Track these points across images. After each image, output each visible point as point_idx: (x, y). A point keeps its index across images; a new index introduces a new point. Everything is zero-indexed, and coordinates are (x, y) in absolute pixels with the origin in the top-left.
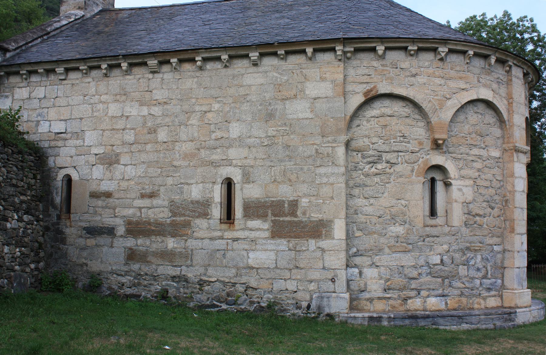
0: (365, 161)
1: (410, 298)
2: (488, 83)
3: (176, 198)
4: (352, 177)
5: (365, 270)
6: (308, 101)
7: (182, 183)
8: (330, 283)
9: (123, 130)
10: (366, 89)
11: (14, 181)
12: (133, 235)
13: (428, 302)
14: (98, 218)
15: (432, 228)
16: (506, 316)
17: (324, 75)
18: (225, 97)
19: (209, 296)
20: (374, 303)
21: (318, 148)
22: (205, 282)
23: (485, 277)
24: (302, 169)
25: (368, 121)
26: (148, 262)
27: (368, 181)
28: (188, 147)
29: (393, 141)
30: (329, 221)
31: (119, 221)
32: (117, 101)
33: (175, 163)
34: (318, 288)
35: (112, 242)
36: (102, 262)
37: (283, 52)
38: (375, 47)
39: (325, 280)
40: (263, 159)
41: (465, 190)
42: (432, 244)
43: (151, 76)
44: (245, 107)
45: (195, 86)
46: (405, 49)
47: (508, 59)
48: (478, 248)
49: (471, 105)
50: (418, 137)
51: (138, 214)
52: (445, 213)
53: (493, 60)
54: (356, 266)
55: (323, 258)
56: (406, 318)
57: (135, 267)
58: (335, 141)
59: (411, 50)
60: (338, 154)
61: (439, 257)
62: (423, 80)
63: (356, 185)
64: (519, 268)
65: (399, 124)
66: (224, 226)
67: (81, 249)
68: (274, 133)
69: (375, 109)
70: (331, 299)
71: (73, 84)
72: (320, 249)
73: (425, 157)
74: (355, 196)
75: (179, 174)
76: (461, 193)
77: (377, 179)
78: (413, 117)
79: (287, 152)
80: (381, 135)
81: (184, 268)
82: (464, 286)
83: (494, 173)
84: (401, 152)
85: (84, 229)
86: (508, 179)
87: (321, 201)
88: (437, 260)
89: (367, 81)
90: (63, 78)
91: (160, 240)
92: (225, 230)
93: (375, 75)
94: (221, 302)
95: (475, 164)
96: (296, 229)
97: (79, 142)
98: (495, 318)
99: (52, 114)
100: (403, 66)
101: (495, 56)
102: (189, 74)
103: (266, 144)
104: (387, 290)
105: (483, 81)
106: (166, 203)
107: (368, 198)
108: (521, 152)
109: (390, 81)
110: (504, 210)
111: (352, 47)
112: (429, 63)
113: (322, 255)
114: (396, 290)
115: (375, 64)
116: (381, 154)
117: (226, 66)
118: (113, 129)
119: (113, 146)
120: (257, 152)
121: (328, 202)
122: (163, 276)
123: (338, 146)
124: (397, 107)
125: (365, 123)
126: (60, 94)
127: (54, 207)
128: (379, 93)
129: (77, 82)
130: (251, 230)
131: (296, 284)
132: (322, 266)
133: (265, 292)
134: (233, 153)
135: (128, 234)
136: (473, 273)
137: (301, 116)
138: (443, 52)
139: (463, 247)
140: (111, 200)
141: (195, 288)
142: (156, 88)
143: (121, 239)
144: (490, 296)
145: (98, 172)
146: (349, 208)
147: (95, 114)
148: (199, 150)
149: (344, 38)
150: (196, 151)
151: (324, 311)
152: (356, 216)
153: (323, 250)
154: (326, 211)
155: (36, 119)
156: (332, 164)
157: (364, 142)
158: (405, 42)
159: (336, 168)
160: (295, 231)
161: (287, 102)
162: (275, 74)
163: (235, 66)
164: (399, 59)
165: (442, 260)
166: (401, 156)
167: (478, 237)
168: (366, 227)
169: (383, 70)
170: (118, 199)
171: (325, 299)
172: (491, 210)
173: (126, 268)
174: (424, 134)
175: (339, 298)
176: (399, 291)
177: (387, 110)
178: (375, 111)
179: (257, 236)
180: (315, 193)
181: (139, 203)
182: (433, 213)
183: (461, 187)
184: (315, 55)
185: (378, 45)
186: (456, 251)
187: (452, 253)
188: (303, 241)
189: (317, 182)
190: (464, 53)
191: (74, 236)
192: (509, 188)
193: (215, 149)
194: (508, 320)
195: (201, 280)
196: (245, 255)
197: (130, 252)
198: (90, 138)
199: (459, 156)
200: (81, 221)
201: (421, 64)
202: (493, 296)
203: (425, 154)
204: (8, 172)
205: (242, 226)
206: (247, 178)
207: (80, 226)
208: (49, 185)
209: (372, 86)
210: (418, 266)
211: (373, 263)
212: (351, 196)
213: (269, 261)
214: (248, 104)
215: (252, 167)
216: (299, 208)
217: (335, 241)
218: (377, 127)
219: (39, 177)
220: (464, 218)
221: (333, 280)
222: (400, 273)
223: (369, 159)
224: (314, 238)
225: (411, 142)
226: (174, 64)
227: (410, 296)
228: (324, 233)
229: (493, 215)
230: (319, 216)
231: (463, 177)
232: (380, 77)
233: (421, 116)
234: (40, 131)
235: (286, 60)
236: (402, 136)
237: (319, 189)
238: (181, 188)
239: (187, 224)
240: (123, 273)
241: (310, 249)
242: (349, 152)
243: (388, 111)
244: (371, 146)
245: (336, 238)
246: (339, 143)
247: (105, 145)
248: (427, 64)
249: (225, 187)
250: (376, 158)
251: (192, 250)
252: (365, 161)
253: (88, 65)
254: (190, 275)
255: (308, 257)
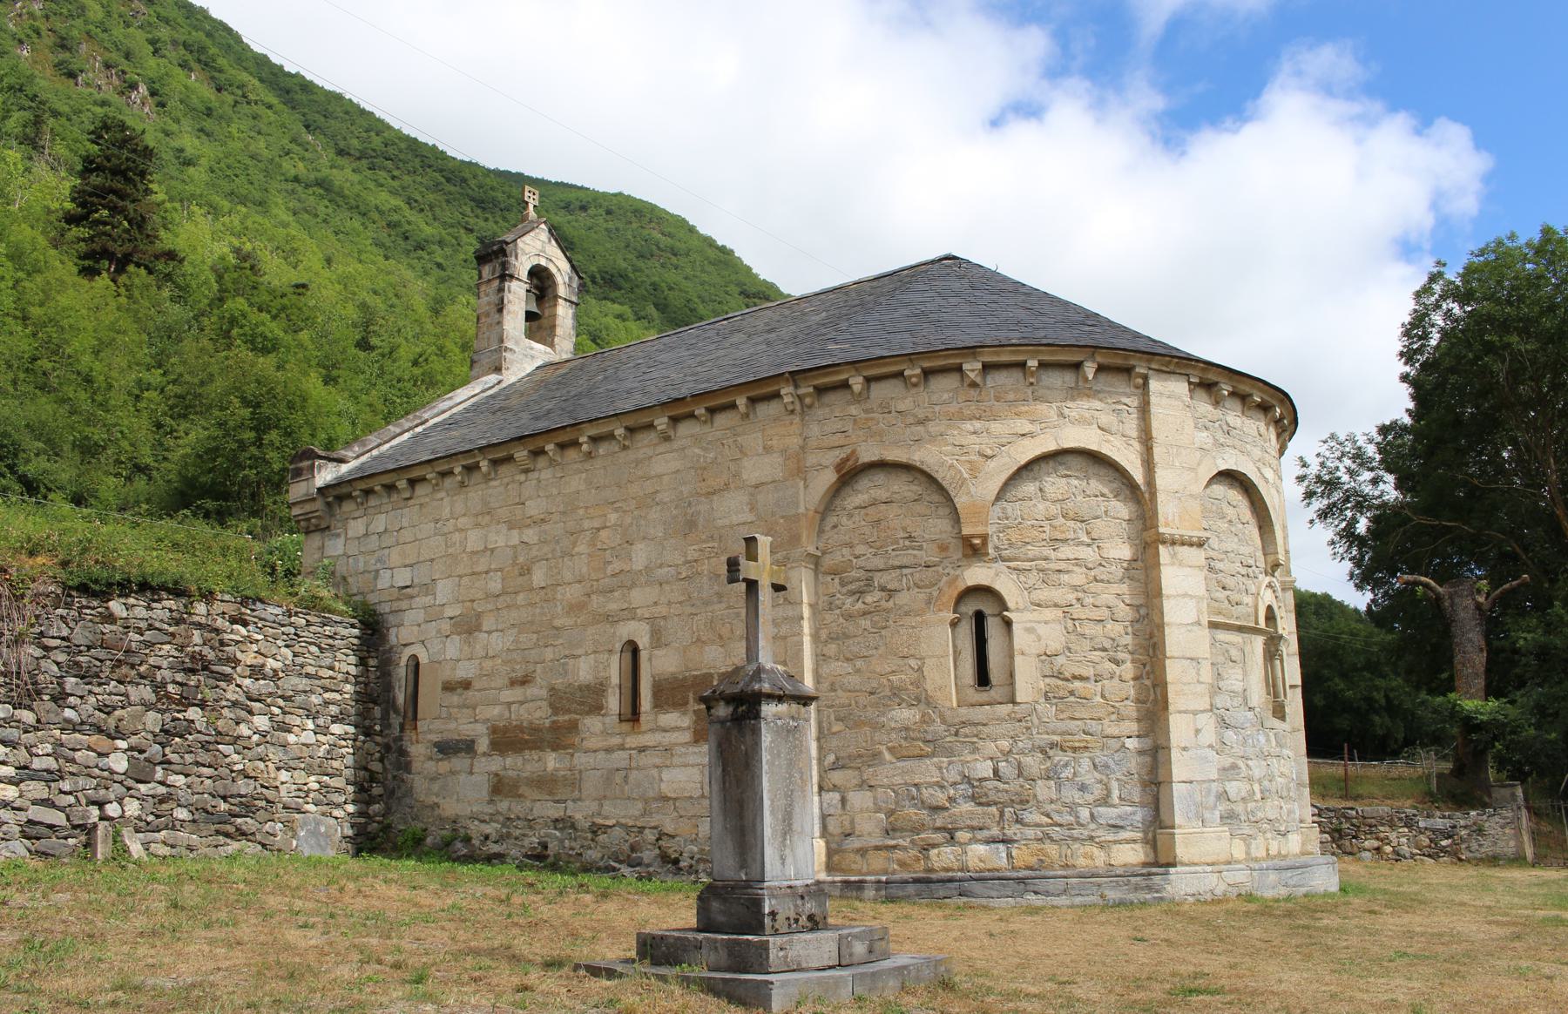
0: (844, 590)
1: (934, 846)
2: (1087, 415)
3: (559, 682)
5: (851, 796)
7: (566, 656)
9: (487, 573)
11: (310, 670)
12: (500, 751)
13: (970, 853)
14: (453, 725)
15: (971, 709)
18: (625, 500)
19: (605, 851)
22: (601, 827)
23: (1105, 801)
25: (850, 516)
26: (520, 796)
28: (572, 593)
31: (481, 729)
32: (477, 525)
33: (558, 623)
35: (472, 765)
36: (458, 800)
37: (1036, 364)
38: (847, 380)
40: (680, 603)
41: (1042, 630)
43: (522, 477)
44: (654, 514)
45: (582, 487)
46: (899, 375)
47: (1132, 362)
48: (1082, 745)
49: (1051, 463)
51: (507, 714)
53: (1090, 369)
54: (835, 788)
57: (503, 805)
59: (911, 376)
61: (989, 763)
64: (1191, 782)
66: (626, 727)
67: (432, 779)
68: (696, 555)
69: (860, 492)
71: (421, 505)
73: (952, 572)
75: (561, 641)
77: (865, 623)
79: (716, 587)
81: (570, 803)
82: (1050, 821)
84: (906, 567)
85: (436, 745)
88: (984, 769)
89: (841, 443)
90: (408, 496)
91: (536, 758)
92: (627, 734)
94: (621, 862)
95: (1065, 578)
97: (428, 600)
99: (395, 557)
100: (901, 407)
101: (1094, 361)
102: (576, 466)
103: (684, 575)
106: (544, 693)
108: (1183, 544)
114: (906, 830)
117: (625, 448)
118: (473, 574)
119: (473, 601)
120: (672, 591)
122: (540, 821)
124: (900, 486)
125: (844, 520)
126: (405, 524)
127: (397, 711)
128: (860, 462)
129: (427, 500)
130: (665, 731)
133: (685, 841)
134: (639, 597)
135: (493, 749)
136: (1071, 794)
137: (735, 519)
138: (973, 370)
139: (1042, 744)
140: (470, 693)
141: (586, 839)
142: (530, 498)
143: (483, 759)
144: (1115, 842)
145: (453, 647)
147: (450, 551)
148: (589, 595)
149: (790, 373)
150: (585, 599)
155: (375, 568)
158: (896, 363)
161: (715, 498)
162: (696, 451)
163: (640, 445)
165: (996, 772)
167: (1079, 722)
169: (866, 419)
170: (479, 690)
173: (490, 809)
179: (673, 741)
181: (508, 695)
182: (983, 679)
184: (869, 388)
191: (422, 758)
192: (1156, 619)
193: (611, 591)
195: (594, 824)
196: (656, 775)
197: (495, 780)
198: (444, 591)
199: (1027, 565)
200: (430, 731)
201: (934, 398)
202: (1128, 841)
204: (295, 655)
205: (652, 725)
206: (658, 640)
207: (429, 741)
208: (390, 675)
209: (849, 451)
211: (863, 781)
213: (692, 785)
214: (659, 508)
215: (664, 618)
219: (372, 662)
222: (913, 798)
226: (551, 454)
227: (931, 842)
232: (861, 433)
234: (379, 587)
235: (712, 423)
238: (564, 664)
239: (573, 727)
240: (487, 818)
243: (882, 494)
247: (463, 602)
249: (628, 656)
251: (580, 772)
252: (844, 590)
253: (437, 470)
254: (578, 816)
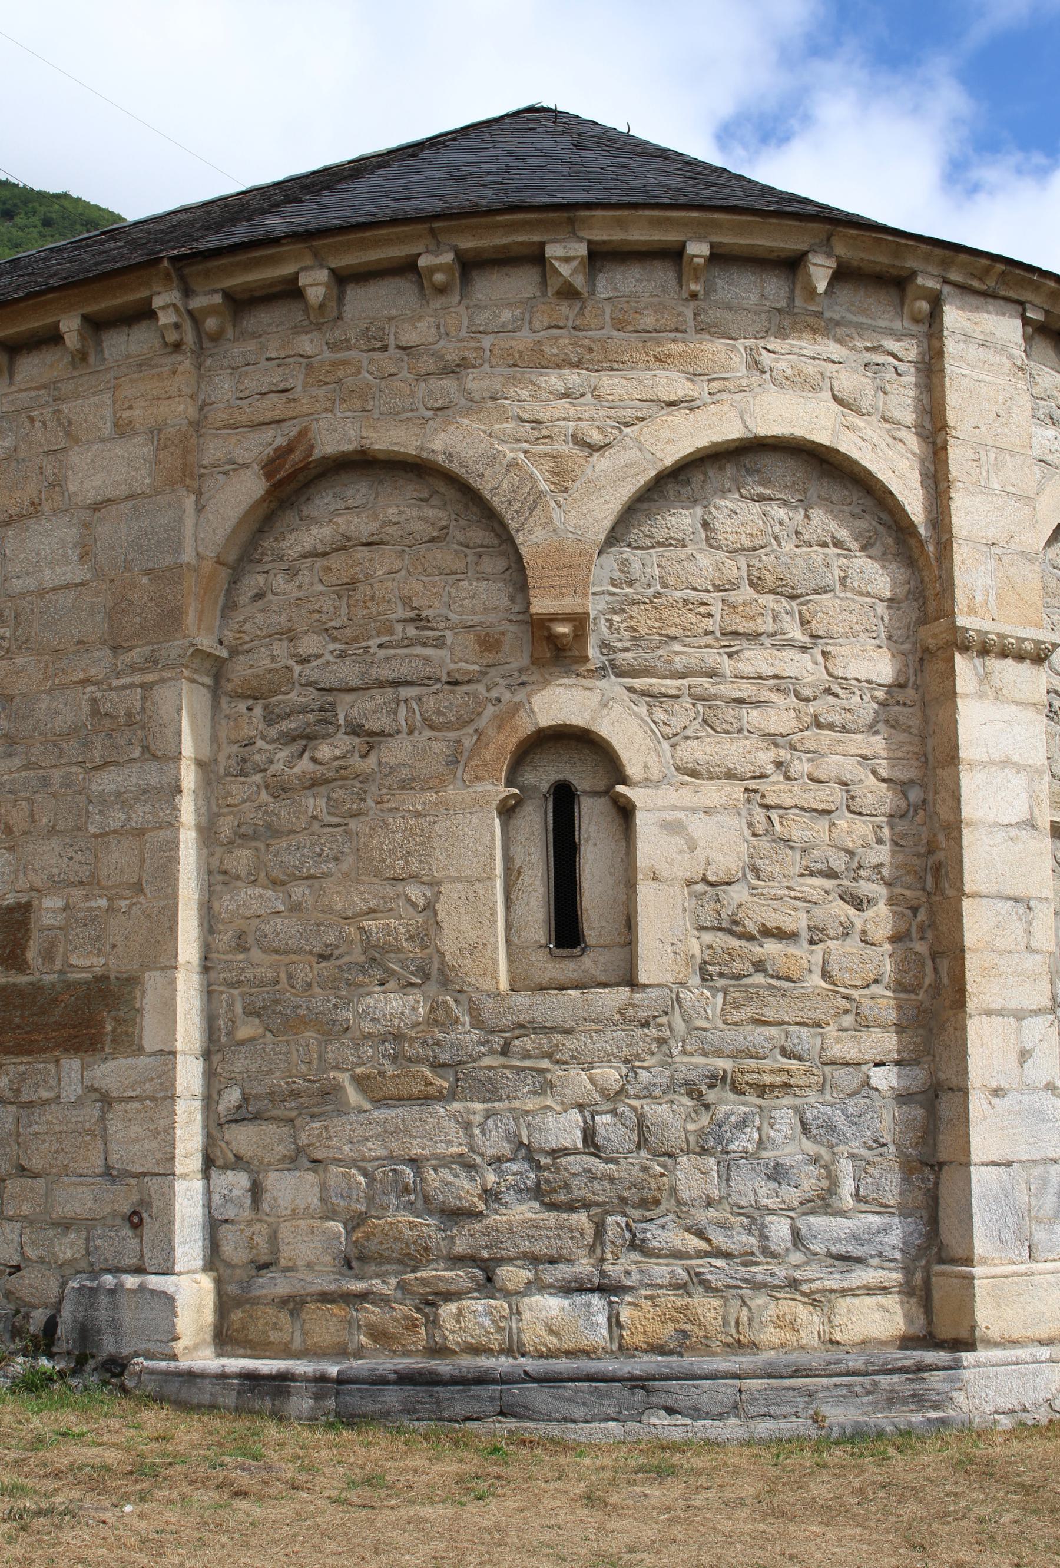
0: (273, 732)
1: (449, 1296)
4: (230, 801)
5: (272, 1180)
6: (75, 521)
8: (127, 1232)
10: (274, 446)
16: (895, 1378)
17: (126, 414)
20: (303, 1316)
21: (99, 695)
24: (46, 782)
25: (292, 573)
27: (284, 813)
29: (378, 641)
30: (128, 980)
34: (88, 1253)
39: (109, 1221)
41: (699, 827)
42: (545, 1064)
46: (408, 268)
47: (911, 264)
48: (778, 1079)
50: (477, 619)
52: (625, 931)
55: (105, 1129)
56: (387, 1383)
58: (152, 662)
59: (433, 270)
60: (162, 712)
61: (575, 1115)
62: (485, 383)
63: (243, 829)
64: (1009, 1164)
65: (403, 572)
69: (315, 521)
70: (123, 1300)
72: (96, 1096)
74: (238, 878)
76: (679, 842)
77: (315, 803)
78: (460, 537)
80: (333, 624)
82: (704, 1246)
83: (868, 752)
84: (408, 683)
86: (939, 771)
87: (103, 903)
89: (277, 414)
93: (306, 385)
95: (753, 716)
96: (22, 1017)
98: (827, 1388)
100: (409, 337)
101: (829, 255)
104: (354, 1264)
105: (782, 365)
107: (283, 883)
108: (1004, 655)
109: (357, 404)
110: (931, 912)
111: (215, 291)
112: (517, 312)
113: (103, 1118)
115: (307, 343)
116: (331, 699)
121: (124, 903)
123: (163, 680)
125: (279, 582)
131: (16, 1238)
132: (100, 1162)
137: (49, 577)
138: (567, 260)
139: (691, 1075)
146: (220, 926)
151: (99, 1345)
152: (241, 957)
153: (106, 1100)
154: (119, 940)
156: (143, 753)
157: (273, 658)
159: (155, 766)
160: (18, 1027)
164: (394, 313)
165: (589, 1135)
166: (406, 701)
167: (773, 1031)
168: (276, 1002)
169: (334, 364)
171: (103, 1299)
172: (852, 911)
174: (506, 601)
175: (148, 1296)
176: (400, 1268)
177: (356, 520)
178: (315, 530)
180: (85, 873)
183: (680, 815)
185: (304, 269)
186: (658, 1092)
187: (636, 1103)
188: (42, 1066)
189: (92, 829)
190: (674, 255)
194: (904, 1401)
199: (671, 685)
201: (482, 318)
202: (870, 1291)
203: (508, 687)
209: (294, 432)
210: (479, 1160)
211: (299, 1150)
212: (226, 878)
216: (35, 934)
217: (144, 1061)
218: (321, 593)
220: (696, 950)
221: (136, 1220)
223: (285, 725)
224: (77, 1050)
225: (449, 642)
228: (109, 1028)
229: (864, 932)
230: (95, 960)
231: (694, 774)
232: (321, 393)
233: (493, 530)
236: (412, 620)
237: (96, 856)
241: (64, 1094)
242: (224, 701)
243: (362, 526)
244: (297, 668)
245: (148, 1048)
246: (167, 667)
248: (506, 315)
250: (311, 718)
252: (273, 732)
255: (57, 1128)
